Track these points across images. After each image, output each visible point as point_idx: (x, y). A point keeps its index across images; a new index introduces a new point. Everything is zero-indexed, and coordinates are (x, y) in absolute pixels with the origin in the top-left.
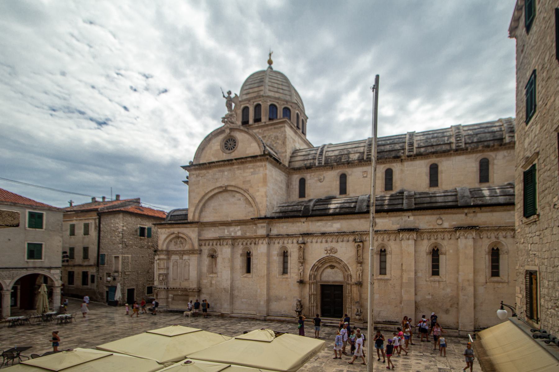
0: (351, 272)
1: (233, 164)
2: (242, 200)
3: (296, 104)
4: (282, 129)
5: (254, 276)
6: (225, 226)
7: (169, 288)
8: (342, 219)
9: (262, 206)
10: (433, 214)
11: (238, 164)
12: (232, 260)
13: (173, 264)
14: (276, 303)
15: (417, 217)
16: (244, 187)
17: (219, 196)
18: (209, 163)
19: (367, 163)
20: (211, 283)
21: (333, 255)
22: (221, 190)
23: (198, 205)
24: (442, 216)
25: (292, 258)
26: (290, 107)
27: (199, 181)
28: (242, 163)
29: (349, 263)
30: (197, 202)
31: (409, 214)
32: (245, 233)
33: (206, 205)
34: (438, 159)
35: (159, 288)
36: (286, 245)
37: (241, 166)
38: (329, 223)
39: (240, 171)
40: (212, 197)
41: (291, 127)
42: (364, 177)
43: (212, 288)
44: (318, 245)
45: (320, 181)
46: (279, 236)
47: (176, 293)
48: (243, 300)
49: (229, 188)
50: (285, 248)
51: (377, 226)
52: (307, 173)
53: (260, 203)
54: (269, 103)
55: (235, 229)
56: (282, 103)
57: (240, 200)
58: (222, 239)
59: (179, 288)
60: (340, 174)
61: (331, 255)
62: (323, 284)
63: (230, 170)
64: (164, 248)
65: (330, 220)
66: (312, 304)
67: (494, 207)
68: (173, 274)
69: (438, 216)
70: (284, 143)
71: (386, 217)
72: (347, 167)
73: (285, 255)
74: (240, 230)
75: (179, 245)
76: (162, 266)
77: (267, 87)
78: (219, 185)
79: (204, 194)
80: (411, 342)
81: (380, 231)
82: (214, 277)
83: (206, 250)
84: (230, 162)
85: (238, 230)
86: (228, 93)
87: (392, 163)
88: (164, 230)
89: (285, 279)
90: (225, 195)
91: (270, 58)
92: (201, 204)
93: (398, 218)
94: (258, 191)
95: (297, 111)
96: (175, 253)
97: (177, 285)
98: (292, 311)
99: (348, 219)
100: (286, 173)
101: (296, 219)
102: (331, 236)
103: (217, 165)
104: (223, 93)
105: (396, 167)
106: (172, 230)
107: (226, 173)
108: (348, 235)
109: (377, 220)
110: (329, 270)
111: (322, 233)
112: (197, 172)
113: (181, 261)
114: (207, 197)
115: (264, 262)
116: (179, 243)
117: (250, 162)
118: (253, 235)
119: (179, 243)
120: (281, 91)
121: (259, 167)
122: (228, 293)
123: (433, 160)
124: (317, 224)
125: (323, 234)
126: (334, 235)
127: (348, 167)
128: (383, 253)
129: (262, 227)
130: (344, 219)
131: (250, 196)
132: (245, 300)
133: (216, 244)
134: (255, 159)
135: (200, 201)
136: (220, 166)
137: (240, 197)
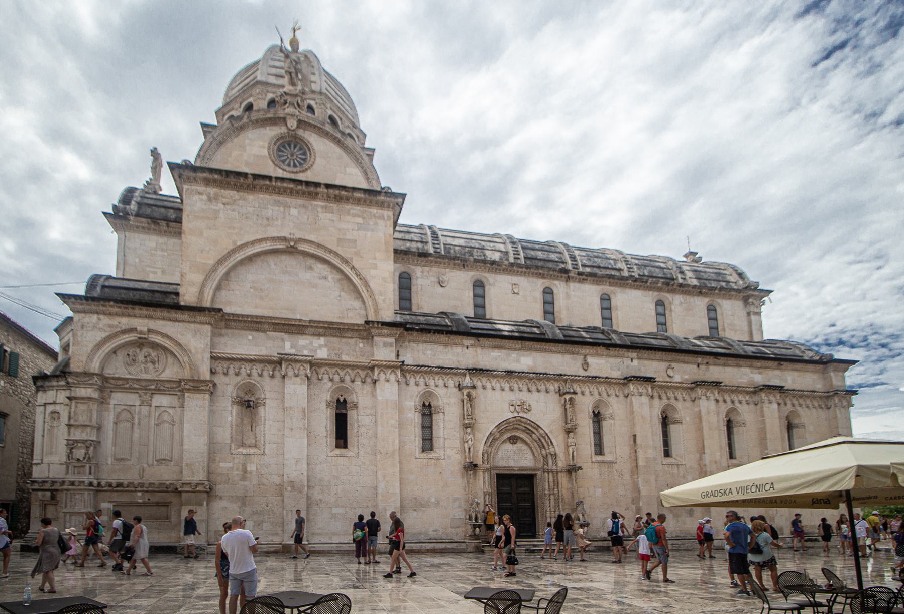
0: (556, 447)
1: (313, 196)
2: (330, 277)
5: (362, 453)
6: (287, 332)
7: (103, 483)
8: (536, 350)
9: (384, 301)
10: (662, 360)
11: (328, 198)
12: (307, 413)
13: (118, 416)
14: (415, 514)
15: (642, 361)
17: (271, 260)
18: (256, 176)
19: (520, 270)
20: (245, 471)
21: (525, 415)
22: (281, 246)
23: (214, 269)
24: (673, 365)
25: (447, 418)
27: (217, 212)
28: (338, 199)
29: (551, 432)
30: (212, 262)
31: (634, 355)
32: (339, 355)
33: (232, 274)
34: (612, 288)
35: (72, 484)
36: (432, 388)
37: (334, 206)
38: (514, 355)
39: (330, 215)
40: (251, 259)
42: (514, 293)
43: (246, 483)
44: (498, 393)
45: (441, 284)
46: (422, 369)
47: (125, 498)
48: (335, 510)
49: (302, 247)
50: (430, 394)
51: (589, 369)
52: (417, 265)
53: (381, 294)
55: (311, 343)
57: (326, 278)
58: (287, 360)
59: (142, 485)
60: (473, 280)
61: (521, 414)
62: (501, 472)
63: (304, 206)
64: (95, 367)
65: (515, 349)
66: (554, 494)
67: (729, 359)
68: (115, 444)
69: (667, 364)
71: (602, 355)
73: (428, 411)
74: (326, 346)
75: (142, 366)
76: (82, 419)
78: (273, 232)
79: (231, 247)
80: (710, 553)
81: (599, 378)
82: (254, 455)
83: (228, 386)
84: (312, 189)
85: (320, 347)
87: (554, 279)
88: (95, 317)
89: (433, 461)
90: (288, 261)
91: (294, 36)
92: (222, 270)
93: (619, 360)
94: (375, 267)
96: (123, 385)
97: (130, 476)
98: (450, 529)
99: (546, 351)
101: (456, 337)
102: (520, 378)
103: (274, 188)
105: (560, 288)
106: (125, 322)
109: (590, 360)
110: (508, 446)
111: (508, 372)
112: (212, 191)
113: (145, 409)
114: (239, 256)
115: (393, 421)
116: (141, 358)
117: (358, 202)
118: (364, 361)
119: (141, 358)
122: (301, 492)
123: (607, 288)
124: (492, 354)
125: (510, 373)
126: (526, 377)
128: (597, 417)
129: (385, 345)
130: (540, 350)
131: (357, 275)
132: (341, 510)
133: (261, 375)
134: (372, 198)
135: (220, 262)
136: (281, 192)
137: (325, 273)
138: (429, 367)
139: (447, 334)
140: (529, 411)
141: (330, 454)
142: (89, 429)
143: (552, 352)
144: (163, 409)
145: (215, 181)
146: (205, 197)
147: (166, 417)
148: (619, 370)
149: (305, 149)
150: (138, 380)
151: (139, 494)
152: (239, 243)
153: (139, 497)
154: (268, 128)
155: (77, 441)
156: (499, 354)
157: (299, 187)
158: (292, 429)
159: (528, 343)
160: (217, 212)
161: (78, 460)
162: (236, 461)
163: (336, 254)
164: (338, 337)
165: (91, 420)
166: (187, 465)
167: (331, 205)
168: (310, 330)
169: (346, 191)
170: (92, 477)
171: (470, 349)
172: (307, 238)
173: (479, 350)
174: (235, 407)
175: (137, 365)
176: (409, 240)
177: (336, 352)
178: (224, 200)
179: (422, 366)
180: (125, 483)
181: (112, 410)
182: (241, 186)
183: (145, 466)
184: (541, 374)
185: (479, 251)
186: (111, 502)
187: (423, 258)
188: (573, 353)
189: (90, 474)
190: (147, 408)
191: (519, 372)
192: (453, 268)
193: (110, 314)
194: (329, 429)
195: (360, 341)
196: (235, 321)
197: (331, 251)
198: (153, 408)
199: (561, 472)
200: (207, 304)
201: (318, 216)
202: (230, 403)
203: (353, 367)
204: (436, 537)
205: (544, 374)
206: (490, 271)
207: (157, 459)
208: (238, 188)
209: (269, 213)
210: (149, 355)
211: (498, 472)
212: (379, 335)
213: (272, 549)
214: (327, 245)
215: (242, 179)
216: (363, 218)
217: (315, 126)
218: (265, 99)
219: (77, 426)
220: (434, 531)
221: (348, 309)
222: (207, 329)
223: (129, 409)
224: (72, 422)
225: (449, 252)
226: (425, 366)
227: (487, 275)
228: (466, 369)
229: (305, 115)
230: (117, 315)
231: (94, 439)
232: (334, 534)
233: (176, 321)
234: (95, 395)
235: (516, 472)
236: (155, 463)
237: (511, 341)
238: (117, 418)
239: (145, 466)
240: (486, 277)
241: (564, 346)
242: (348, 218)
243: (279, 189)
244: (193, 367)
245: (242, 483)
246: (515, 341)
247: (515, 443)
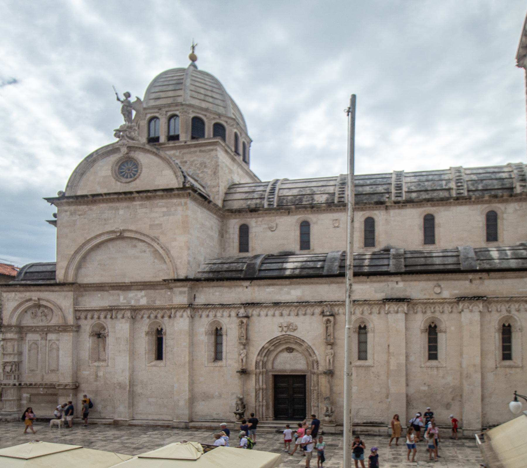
1: (133, 199)
8: (303, 283)
9: (181, 263)
11: (142, 199)
13: (30, 347)
14: (203, 403)
16: (152, 234)
17: (110, 245)
18: (93, 196)
20: (97, 376)
21: (292, 334)
27: (75, 221)
28: (148, 198)
30: (72, 253)
35: (5, 385)
36: (219, 319)
37: (147, 203)
38: (285, 289)
39: (144, 210)
40: (98, 246)
43: (98, 383)
44: (269, 318)
45: (271, 229)
46: (207, 306)
47: (34, 391)
49: (127, 234)
54: (192, 115)
55: (136, 295)
56: (212, 116)
57: (145, 252)
60: (300, 222)
62: (276, 373)
63: (128, 207)
65: (286, 285)
71: (366, 282)
72: (310, 212)
74: (145, 296)
75: (40, 318)
77: (189, 93)
78: (108, 228)
79: (84, 241)
82: (102, 366)
83: (87, 326)
84: (129, 196)
85: (142, 297)
86: (125, 94)
87: (373, 210)
92: (78, 257)
94: (175, 240)
95: (235, 130)
96: (33, 330)
97: (37, 380)
99: (312, 283)
100: (219, 216)
104: (116, 94)
106: (28, 295)
107: (121, 212)
108: (312, 306)
110: (285, 354)
111: (275, 303)
112: (73, 208)
113: (43, 342)
117: (162, 197)
118: (167, 304)
122: (125, 389)
125: (276, 304)
129: (181, 293)
131: (162, 248)
133: (105, 317)
134: (169, 193)
135: (77, 252)
138: (213, 305)
140: (295, 330)
141: (147, 365)
142: (12, 356)
144: (53, 341)
146: (68, 213)
147: (54, 346)
148: (383, 292)
149: (136, 164)
150: (38, 326)
151: (41, 389)
152: (88, 238)
153: (41, 391)
154: (111, 156)
155: (7, 362)
156: (273, 290)
157: (121, 196)
158: (120, 351)
159: (294, 280)
160: (75, 221)
161: (8, 372)
162: (92, 370)
163: (148, 236)
164: (153, 289)
165: (14, 350)
166: (61, 374)
167: (145, 202)
168: (133, 287)
169: (151, 193)
170: (16, 381)
172: (130, 228)
174: (91, 338)
175: (37, 318)
176: (250, 199)
177: (152, 299)
178: (80, 213)
179: (208, 305)
180: (33, 383)
181: (27, 343)
182: (88, 202)
183: (44, 374)
184: (303, 302)
185: (309, 196)
186: (29, 393)
188: (338, 283)
189: (15, 379)
190: (45, 341)
191: (284, 303)
193: (20, 291)
194: (147, 349)
195: (169, 290)
196: (88, 287)
197: (144, 235)
198: (47, 342)
199: (321, 374)
200: (70, 279)
201: (137, 212)
202: (88, 336)
203: (162, 309)
204: (218, 418)
205: (306, 302)
206: (312, 213)
207: (354, 297)
208: (87, 203)
209: (105, 216)
210: (44, 311)
211: (274, 373)
212: (176, 287)
213: (108, 423)
214: (141, 231)
215: (86, 199)
216: (167, 207)
217: (140, 148)
218: (145, 119)
219: (7, 354)
220: (217, 414)
221: (159, 271)
222: (71, 294)
223: (36, 343)
224: (5, 353)
225: (282, 202)
226: (211, 305)
228: (241, 304)
229: (131, 143)
230: (23, 291)
231: (16, 360)
232: (150, 414)
233: (53, 291)
234: (16, 336)
235: (288, 374)
236: (50, 372)
238: (30, 348)
239: (44, 374)
241: (327, 278)
242: (157, 209)
244: (64, 318)
245: (95, 383)
247: (291, 352)
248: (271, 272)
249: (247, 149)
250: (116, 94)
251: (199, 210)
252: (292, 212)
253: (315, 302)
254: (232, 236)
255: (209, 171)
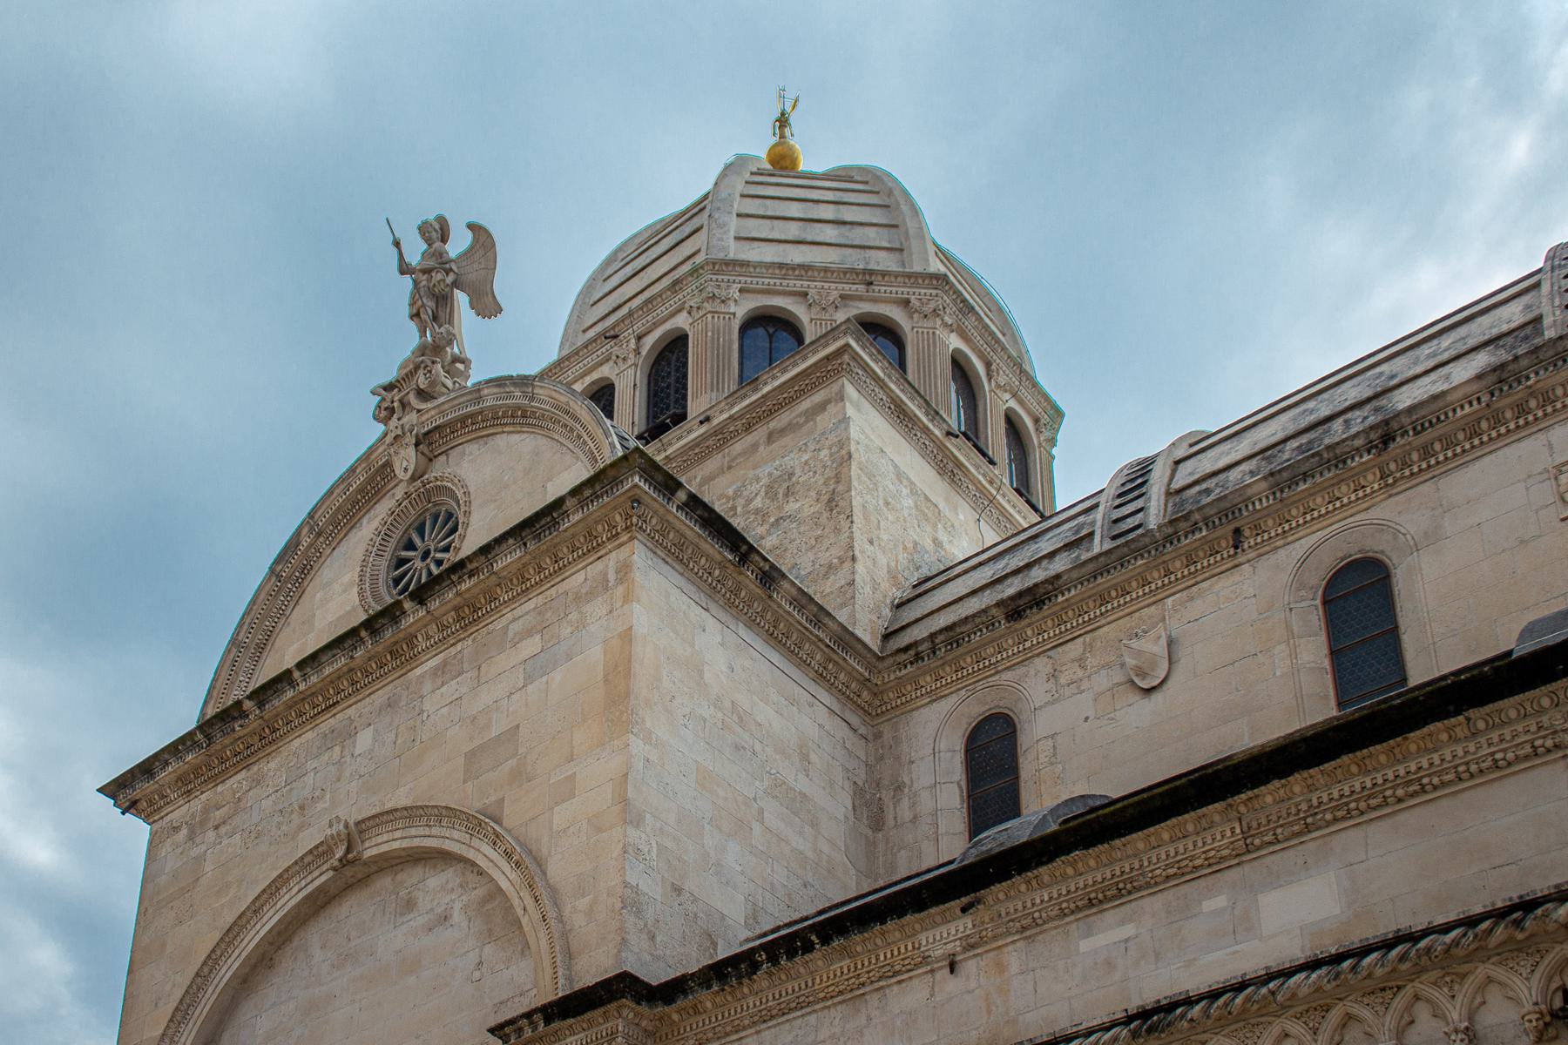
3: (939, 280)
4: (824, 421)
8: (1346, 813)
9: (590, 912)
16: (470, 798)
26: (896, 314)
41: (900, 415)
49: (377, 845)
54: (742, 308)
56: (834, 290)
60: (1317, 578)
65: (1215, 865)
70: (835, 502)
72: (1372, 481)
77: (734, 224)
86: (424, 230)
94: (567, 791)
95: (955, 342)
99: (1419, 789)
100: (846, 697)
104: (397, 244)
107: (364, 740)
108: (1450, 966)
111: (1144, 1014)
120: (830, 233)
121: (578, 598)
124: (1085, 945)
127: (1389, 483)
134: (548, 539)
139: (825, 940)
143: (1465, 776)
145: (196, 771)
156: (1128, 930)
159: (1269, 794)
171: (970, 967)
173: (1014, 956)
187: (1034, 616)
191: (1214, 995)
192: (1195, 578)
205: (1387, 945)
217: (463, 420)
227: (1385, 510)
237: (1164, 830)
240: (1381, 527)
243: (321, 691)
246: (1188, 820)
248: (861, 201)
249: (1036, 457)
250: (397, 244)
251: (711, 623)
252: (1258, 529)
253: (1470, 922)
254: (926, 803)
255: (803, 506)
